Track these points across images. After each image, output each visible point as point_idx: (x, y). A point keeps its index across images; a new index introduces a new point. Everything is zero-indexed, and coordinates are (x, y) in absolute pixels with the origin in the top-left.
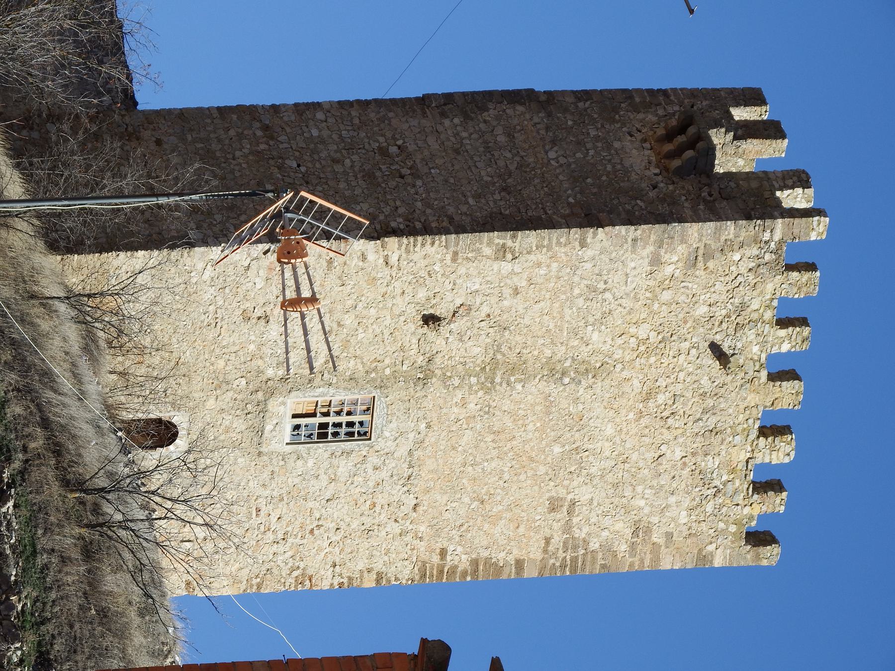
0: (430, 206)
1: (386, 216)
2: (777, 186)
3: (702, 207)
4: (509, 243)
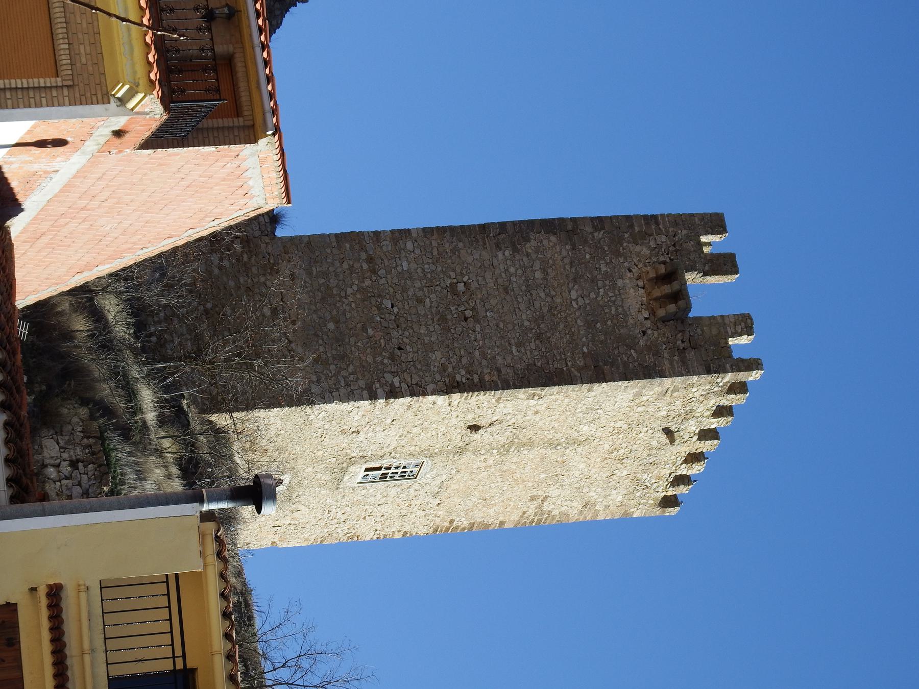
0: (484, 355)
1: (453, 368)
2: (730, 333)
3: (676, 358)
4: (539, 392)
